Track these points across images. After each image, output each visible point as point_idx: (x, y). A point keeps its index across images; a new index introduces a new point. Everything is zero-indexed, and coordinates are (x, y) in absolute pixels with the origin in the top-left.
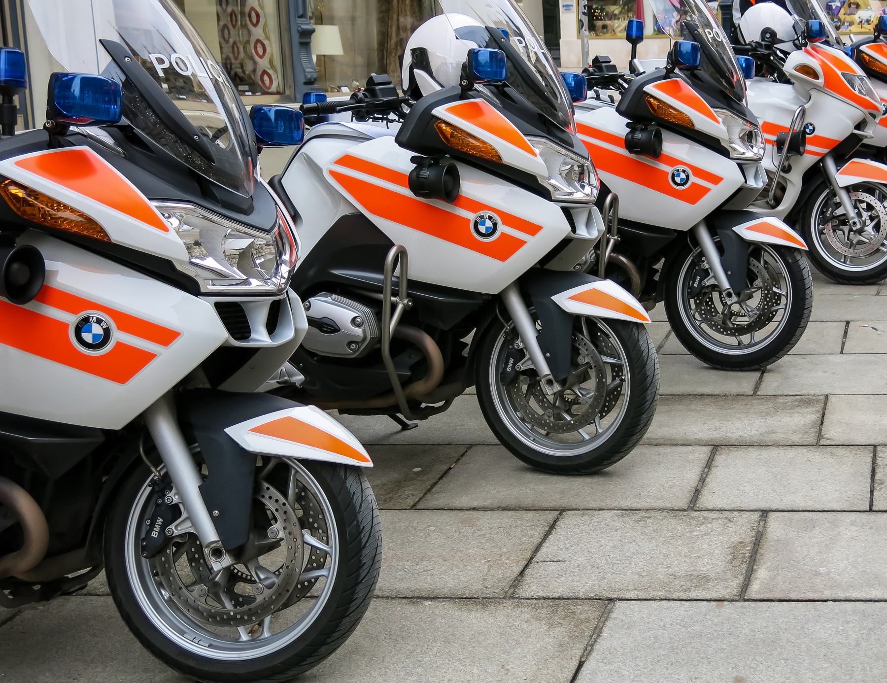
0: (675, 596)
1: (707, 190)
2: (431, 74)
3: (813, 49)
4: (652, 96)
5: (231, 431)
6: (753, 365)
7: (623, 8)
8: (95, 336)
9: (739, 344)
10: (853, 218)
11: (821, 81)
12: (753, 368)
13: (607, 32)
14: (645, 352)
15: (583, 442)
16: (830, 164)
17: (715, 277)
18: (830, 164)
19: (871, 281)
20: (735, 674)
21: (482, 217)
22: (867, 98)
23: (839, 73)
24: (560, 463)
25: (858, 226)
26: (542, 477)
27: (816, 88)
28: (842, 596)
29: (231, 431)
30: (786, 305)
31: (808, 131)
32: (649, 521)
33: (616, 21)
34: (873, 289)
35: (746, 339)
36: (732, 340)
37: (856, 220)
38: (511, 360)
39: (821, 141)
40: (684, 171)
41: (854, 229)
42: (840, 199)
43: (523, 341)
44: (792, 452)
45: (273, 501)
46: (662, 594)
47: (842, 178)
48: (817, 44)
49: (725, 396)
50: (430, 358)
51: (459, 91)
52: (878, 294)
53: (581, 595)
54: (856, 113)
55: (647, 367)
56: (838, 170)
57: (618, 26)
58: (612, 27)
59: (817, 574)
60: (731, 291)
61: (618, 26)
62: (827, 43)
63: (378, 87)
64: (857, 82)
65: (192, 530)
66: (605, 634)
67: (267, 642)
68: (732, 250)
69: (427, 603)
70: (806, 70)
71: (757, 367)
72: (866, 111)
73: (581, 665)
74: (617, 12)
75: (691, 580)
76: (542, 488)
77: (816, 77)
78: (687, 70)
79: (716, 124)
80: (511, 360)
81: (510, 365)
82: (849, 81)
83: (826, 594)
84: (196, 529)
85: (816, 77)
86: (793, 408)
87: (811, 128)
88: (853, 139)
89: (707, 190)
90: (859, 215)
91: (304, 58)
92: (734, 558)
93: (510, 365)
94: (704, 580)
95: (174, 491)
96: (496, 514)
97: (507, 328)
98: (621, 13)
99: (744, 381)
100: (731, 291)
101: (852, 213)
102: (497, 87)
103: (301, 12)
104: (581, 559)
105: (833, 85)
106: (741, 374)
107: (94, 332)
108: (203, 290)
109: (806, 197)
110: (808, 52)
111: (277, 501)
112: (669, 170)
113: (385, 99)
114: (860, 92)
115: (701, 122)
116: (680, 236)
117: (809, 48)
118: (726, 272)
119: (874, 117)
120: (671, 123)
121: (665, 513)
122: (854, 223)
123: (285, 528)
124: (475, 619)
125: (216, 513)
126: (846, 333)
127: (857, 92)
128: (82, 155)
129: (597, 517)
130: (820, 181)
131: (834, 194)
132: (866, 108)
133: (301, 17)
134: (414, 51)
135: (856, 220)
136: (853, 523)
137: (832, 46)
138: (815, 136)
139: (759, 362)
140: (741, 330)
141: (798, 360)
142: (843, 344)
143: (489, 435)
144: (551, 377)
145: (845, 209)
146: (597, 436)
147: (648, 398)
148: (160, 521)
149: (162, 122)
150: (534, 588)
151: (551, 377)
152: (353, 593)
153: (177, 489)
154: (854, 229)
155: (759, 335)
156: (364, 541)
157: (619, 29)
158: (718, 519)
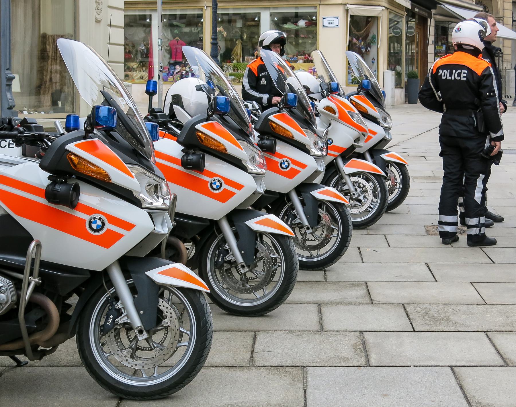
0: (335, 365)
1: (298, 172)
2: (182, 107)
3: (332, 97)
4: (272, 122)
5: (148, 273)
6: (320, 267)
7: (140, 64)
8: (98, 226)
9: (311, 255)
10: (353, 191)
11: (337, 115)
12: (319, 268)
13: (129, 79)
14: (293, 251)
15: (257, 299)
16: (340, 162)
17: (300, 219)
18: (340, 162)
19: (363, 227)
20: (382, 393)
21: (214, 180)
22: (361, 125)
23: (346, 111)
24: (245, 310)
25: (356, 196)
26: (234, 317)
27: (334, 119)
28: (417, 364)
29: (148, 273)
30: (338, 234)
31: (329, 143)
32: (303, 335)
33: (135, 72)
34: (364, 232)
35: (315, 253)
36: (307, 254)
37: (355, 192)
38: (222, 255)
39: (336, 148)
40: (287, 161)
41: (354, 197)
42: (346, 180)
43: (229, 245)
44: (361, 307)
45: (165, 308)
46: (328, 364)
47: (347, 169)
48: (334, 95)
49: (310, 282)
50: (182, 253)
51: (206, 116)
52: (369, 234)
53: (288, 365)
54: (356, 133)
55: (294, 259)
56: (344, 165)
57: (136, 76)
58: (132, 76)
59: (401, 356)
60: (309, 226)
61: (136, 76)
62: (339, 95)
63: (158, 114)
64: (356, 117)
65: (128, 321)
66: (309, 379)
67: (156, 378)
68: (309, 203)
69: (212, 368)
70: (329, 109)
71: (321, 268)
72: (361, 132)
73: (305, 391)
74: (135, 67)
75: (340, 359)
76: (238, 322)
77: (335, 113)
78: (287, 108)
79: (304, 136)
80: (222, 255)
81: (221, 258)
82: (351, 115)
83: (409, 364)
84: (131, 320)
85: (335, 113)
86: (350, 287)
87: (331, 141)
88: (353, 147)
89: (298, 172)
90: (356, 190)
91: (8, 93)
92: (356, 350)
93: (221, 258)
94: (345, 359)
95: (120, 302)
96: (222, 333)
97: (220, 237)
98: (138, 67)
99: (318, 275)
100: (309, 226)
101: (352, 189)
102: (220, 115)
103: (8, 67)
104: (278, 351)
105: (344, 118)
106: (313, 272)
107: (97, 223)
108: (143, 206)
109: (327, 178)
110: (329, 99)
111: (164, 306)
112: (279, 160)
113: (163, 120)
114: (357, 121)
115: (298, 135)
116: (281, 195)
117: (330, 97)
118: (306, 216)
119: (364, 135)
120: (282, 136)
121: (309, 332)
122: (354, 194)
123: (170, 321)
124: (239, 374)
125: (142, 312)
126: (360, 253)
127: (355, 121)
128: (93, 142)
129: (275, 334)
130: (334, 171)
131: (342, 178)
132: (360, 131)
133: (7, 69)
134: (174, 96)
135: (355, 192)
136: (408, 336)
137: (341, 96)
138: (333, 145)
139: (321, 266)
140: (316, 248)
141: (341, 265)
142: (362, 258)
143: (180, 302)
144: (244, 264)
145: (349, 186)
146: (264, 296)
147: (294, 275)
148: (112, 317)
149: (126, 128)
150: (262, 362)
151: (244, 264)
152: (203, 352)
153: (122, 301)
154: (354, 197)
155: (323, 251)
156: (208, 327)
157: (137, 78)
158: (339, 334)
